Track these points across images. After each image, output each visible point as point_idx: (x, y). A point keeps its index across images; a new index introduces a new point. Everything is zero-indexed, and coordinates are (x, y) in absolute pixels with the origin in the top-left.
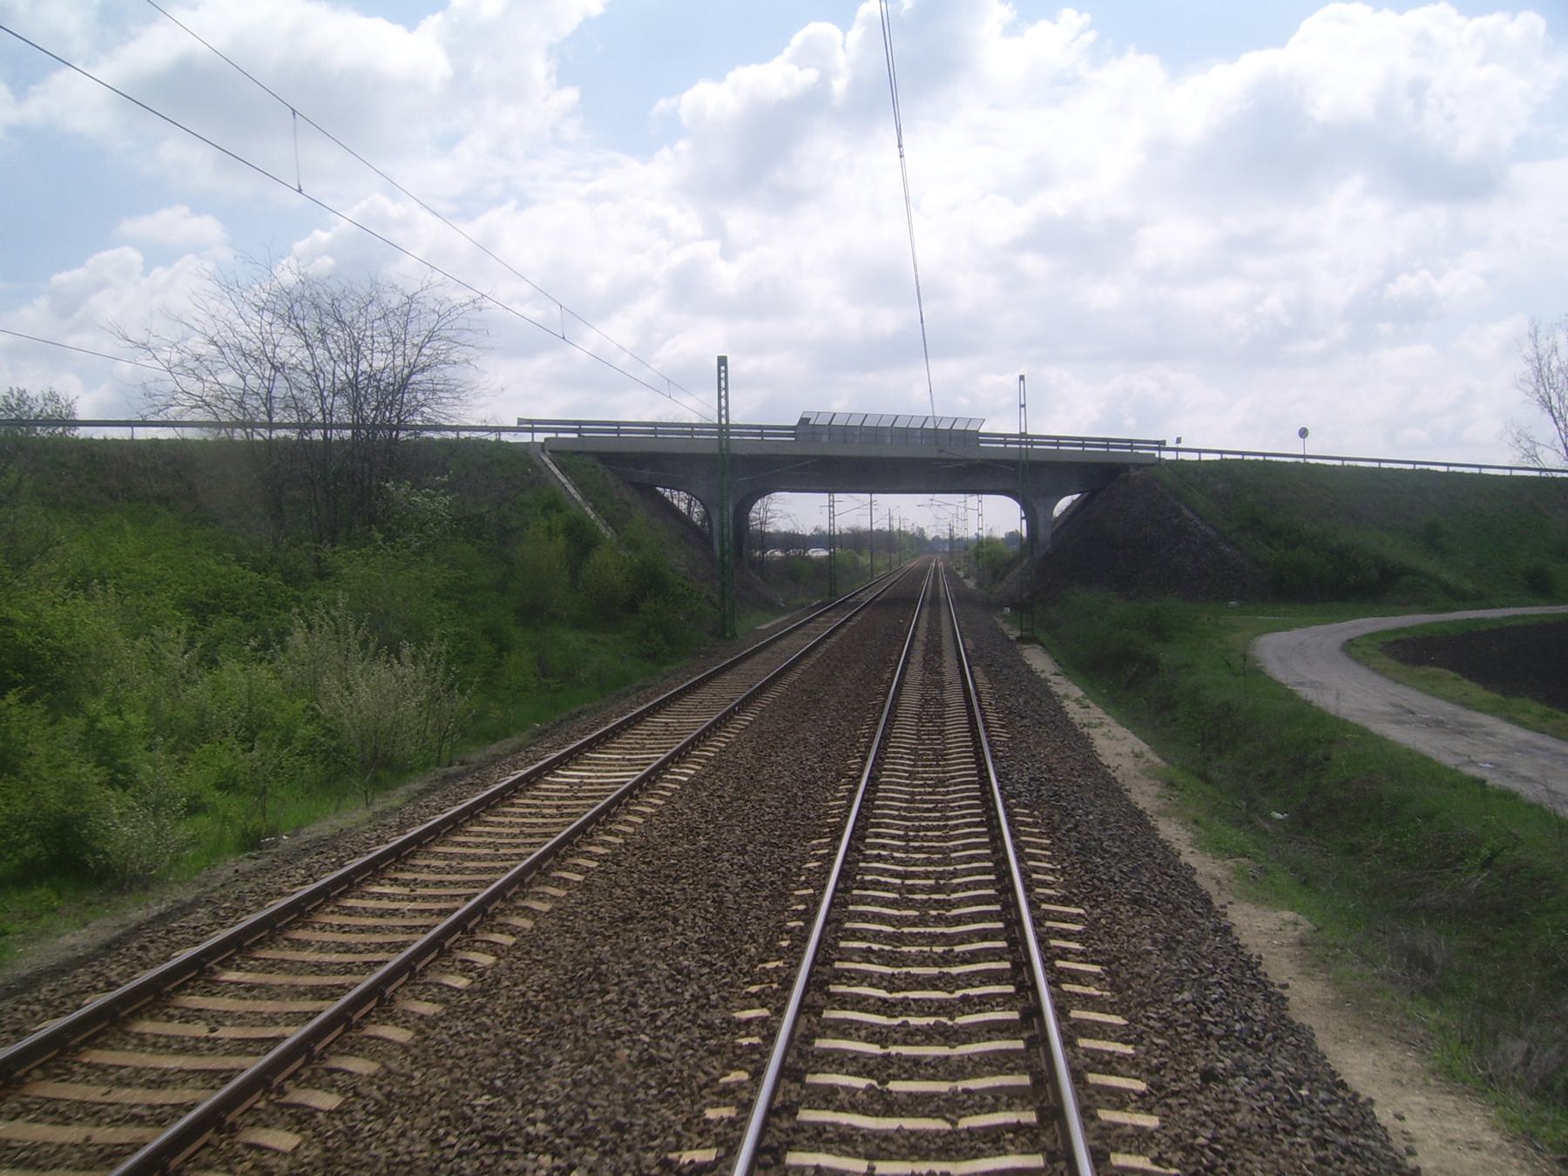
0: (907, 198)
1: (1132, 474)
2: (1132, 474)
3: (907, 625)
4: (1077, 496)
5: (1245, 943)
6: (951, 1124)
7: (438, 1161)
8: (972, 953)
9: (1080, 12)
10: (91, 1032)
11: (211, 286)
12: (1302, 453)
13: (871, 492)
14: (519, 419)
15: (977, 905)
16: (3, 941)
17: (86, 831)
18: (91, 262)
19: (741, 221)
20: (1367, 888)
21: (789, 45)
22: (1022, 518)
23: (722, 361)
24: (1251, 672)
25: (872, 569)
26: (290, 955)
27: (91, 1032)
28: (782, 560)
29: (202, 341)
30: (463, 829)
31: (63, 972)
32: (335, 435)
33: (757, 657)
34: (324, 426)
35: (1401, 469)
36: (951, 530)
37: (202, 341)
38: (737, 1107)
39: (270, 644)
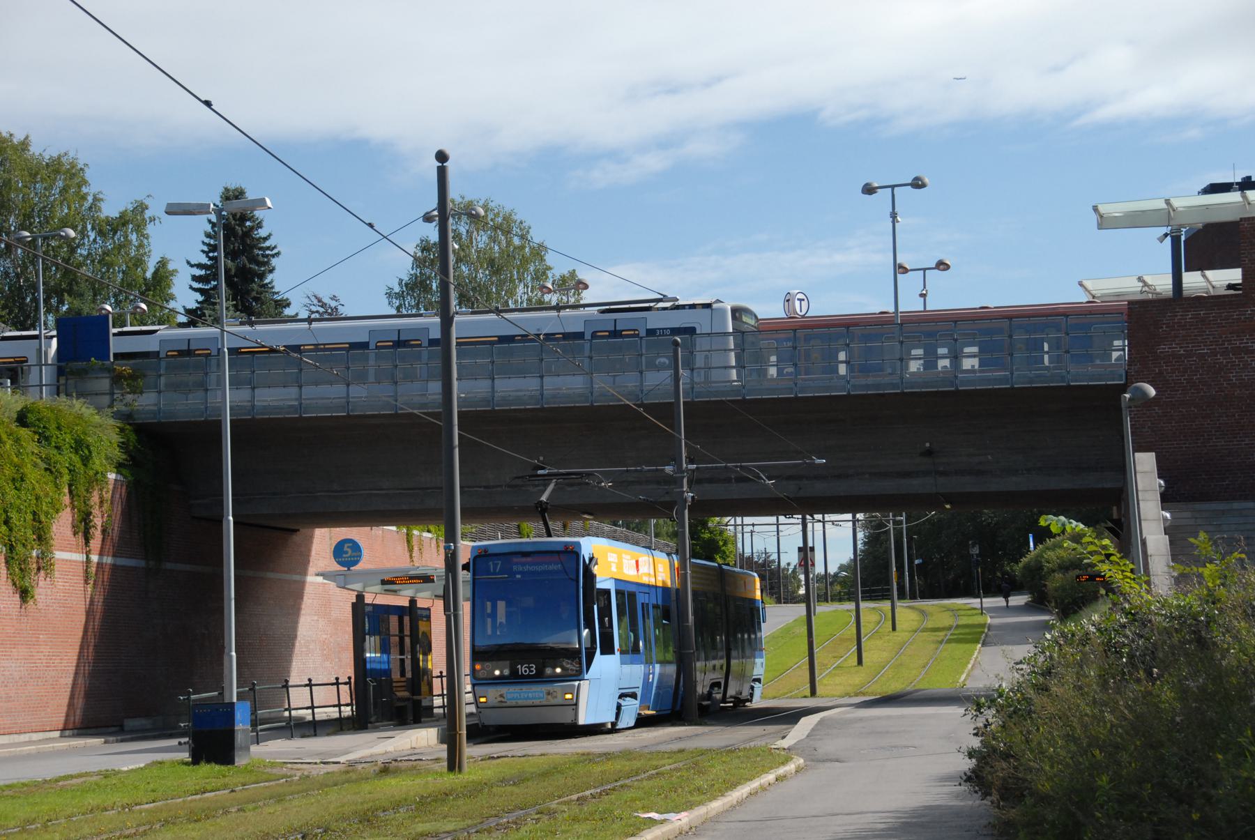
0: (894, 216)
1: (345, 550)
2: (345, 550)
3: (265, 690)
4: (655, 712)
5: (307, 680)
6: (108, 221)
7: (21, 388)
8: (909, 336)
9: (202, 296)
10: (980, 579)
11: (965, 788)
12: (781, 551)
13: (330, 527)
14: (1158, 239)
15: (617, 605)
16: (535, 839)
17: (1021, 539)
18: (804, 587)
19: (33, 378)
20: (1173, 615)
21: (1006, 597)
22: (792, 517)
23: (442, 157)
24: (217, 220)
25: (75, 729)
26: (848, 827)
27: (980, 579)
28: (464, 397)
29: (77, 721)
30: (1008, 760)
31: (47, 739)
32: (1126, 344)
33: (976, 623)
34: (362, 803)
35: (891, 549)
36: (371, 529)
37: (77, 721)
38: (755, 658)
39: (106, 545)
